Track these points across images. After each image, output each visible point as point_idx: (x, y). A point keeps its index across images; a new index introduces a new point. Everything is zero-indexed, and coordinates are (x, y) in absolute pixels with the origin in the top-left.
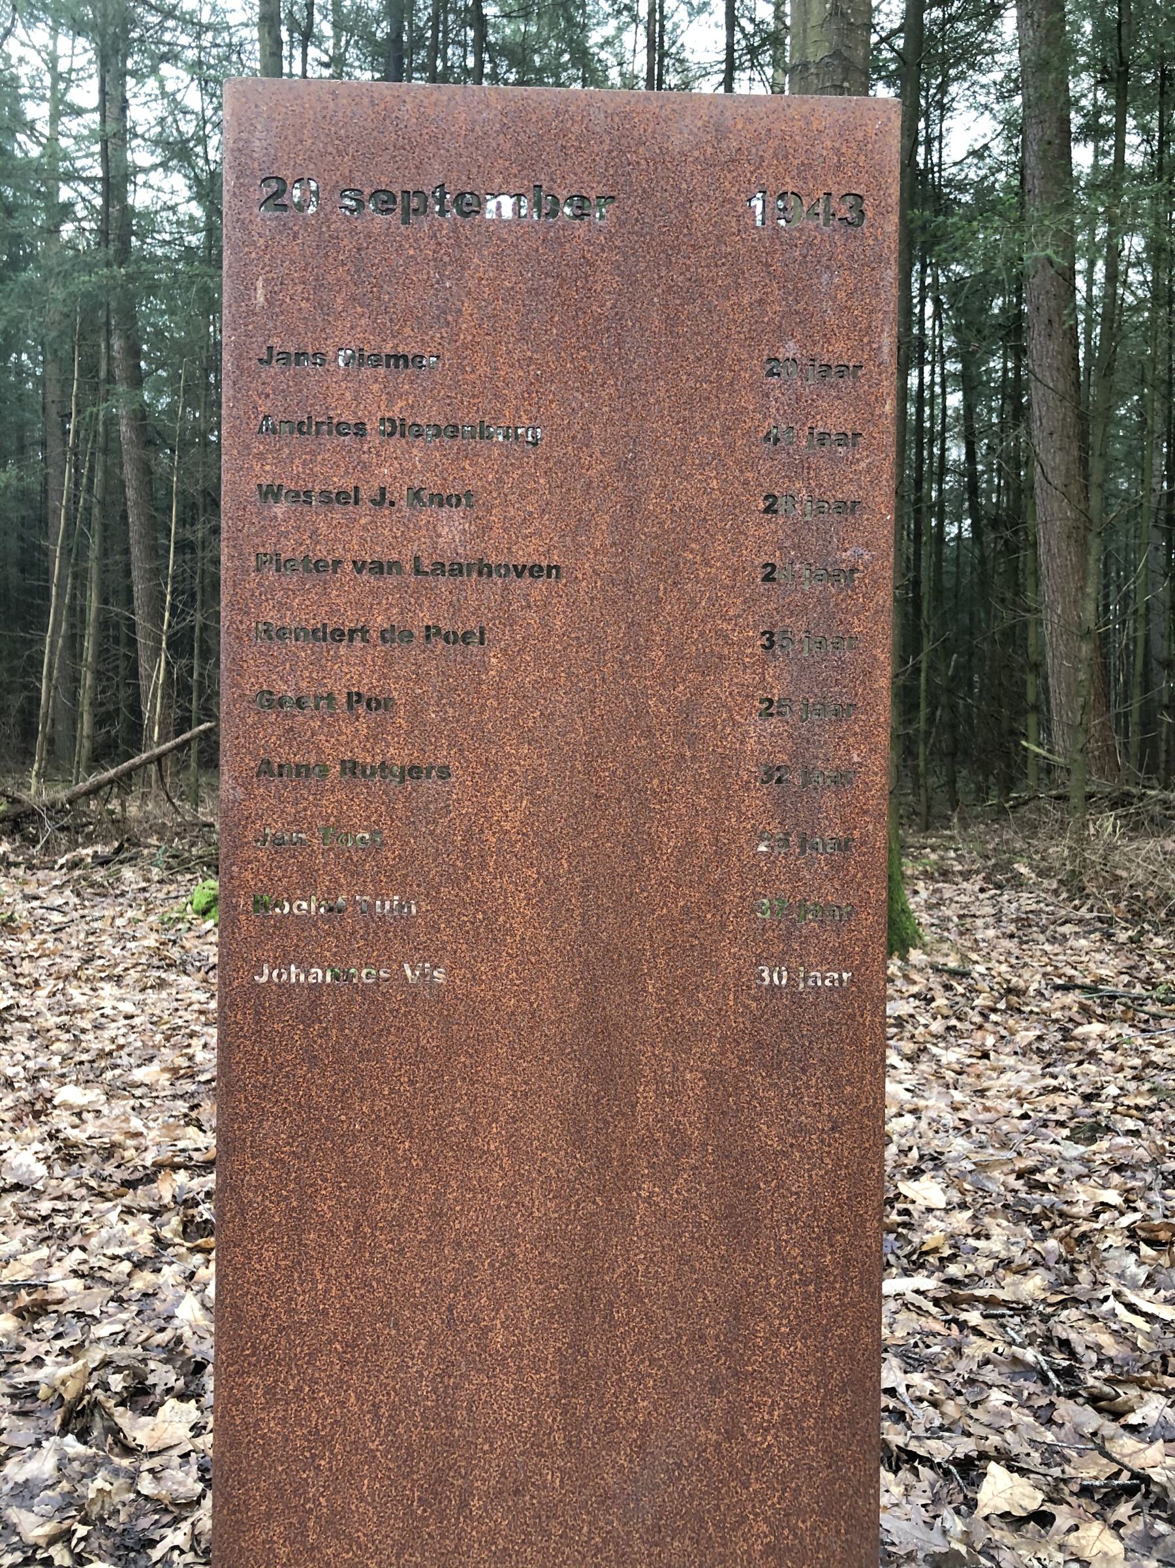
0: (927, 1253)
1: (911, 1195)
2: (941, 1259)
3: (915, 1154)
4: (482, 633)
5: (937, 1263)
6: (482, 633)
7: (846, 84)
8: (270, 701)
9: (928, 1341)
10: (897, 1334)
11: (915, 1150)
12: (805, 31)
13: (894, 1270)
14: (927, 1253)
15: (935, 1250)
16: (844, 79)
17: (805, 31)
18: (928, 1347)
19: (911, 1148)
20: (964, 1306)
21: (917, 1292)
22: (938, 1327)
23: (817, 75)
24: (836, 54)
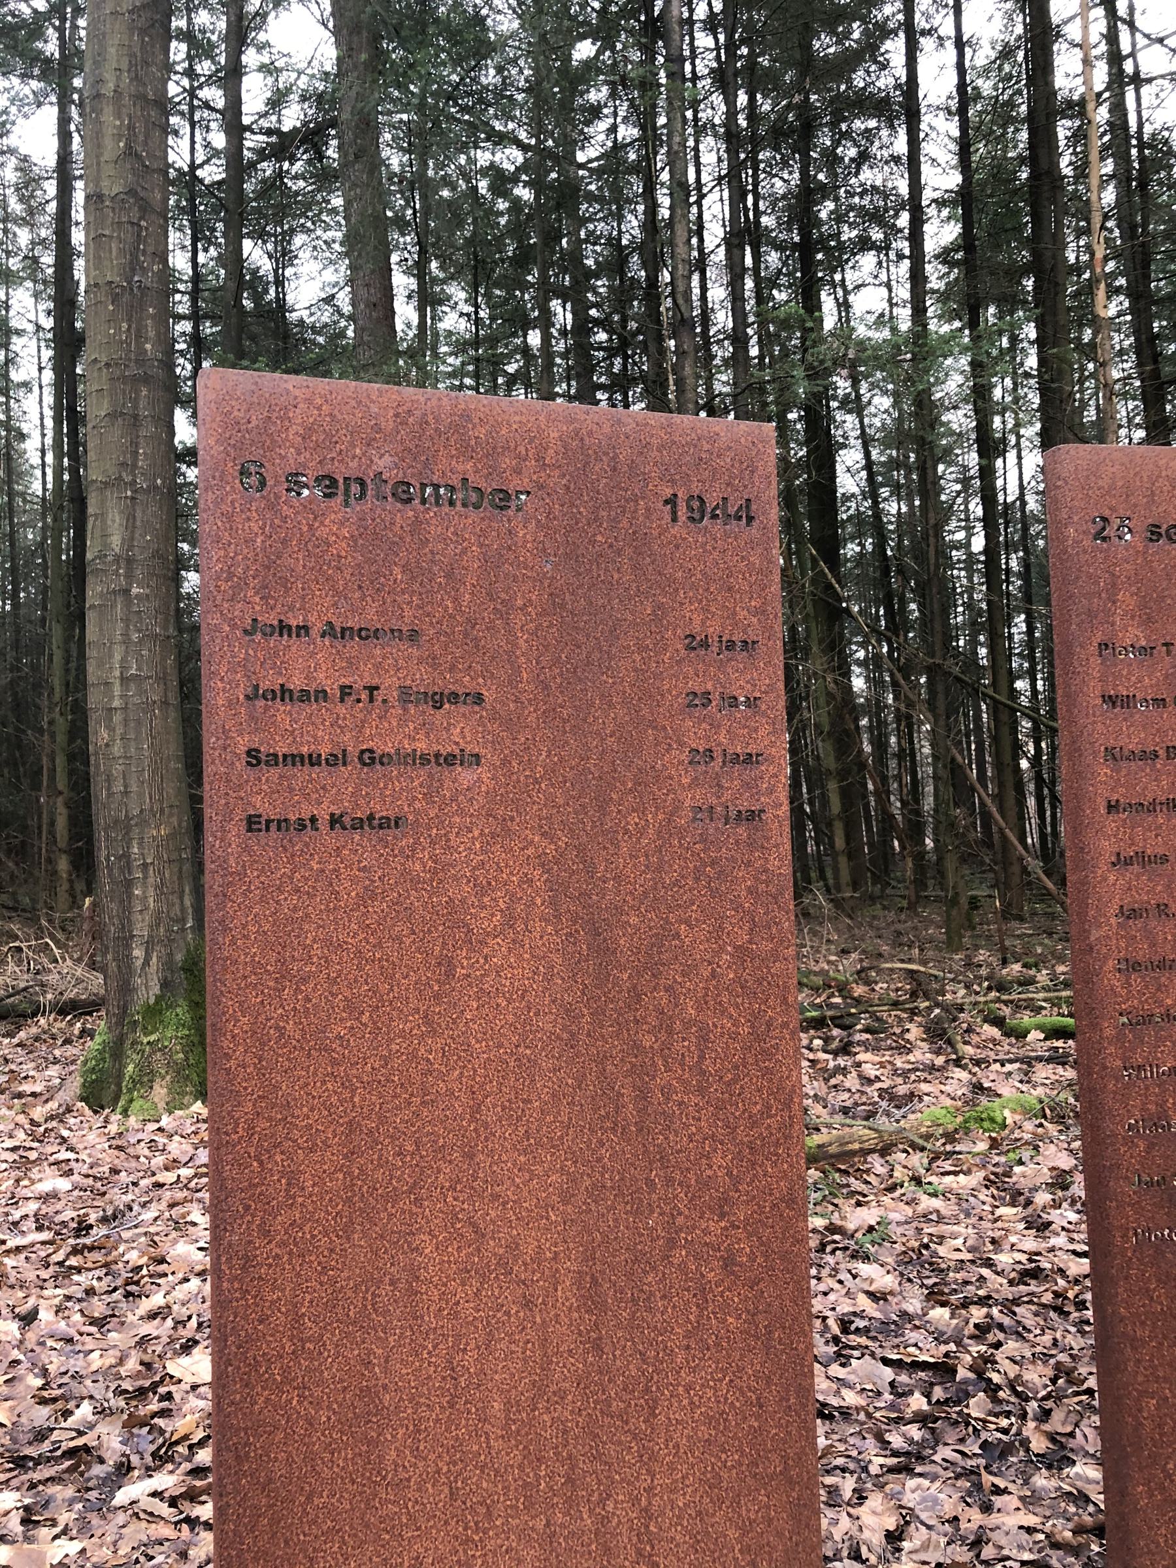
0: (177, 1443)
1: (177, 1374)
2: (191, 1447)
3: (194, 1323)
4: (344, 756)
5: (186, 1452)
6: (344, 756)
7: (143, 223)
8: (1113, 755)
9: (150, 1552)
10: (121, 1552)
11: (194, 1318)
12: (98, 164)
13: (136, 1473)
14: (177, 1443)
15: (186, 1437)
16: (140, 219)
17: (98, 164)
18: (152, 1558)
19: (190, 1317)
20: (203, 1498)
21: (154, 1494)
22: (167, 1531)
23: (113, 209)
24: (132, 192)
